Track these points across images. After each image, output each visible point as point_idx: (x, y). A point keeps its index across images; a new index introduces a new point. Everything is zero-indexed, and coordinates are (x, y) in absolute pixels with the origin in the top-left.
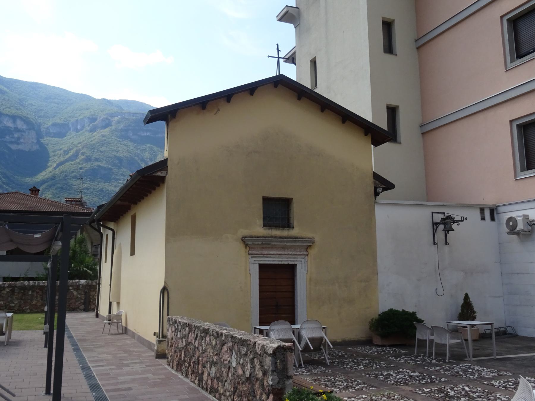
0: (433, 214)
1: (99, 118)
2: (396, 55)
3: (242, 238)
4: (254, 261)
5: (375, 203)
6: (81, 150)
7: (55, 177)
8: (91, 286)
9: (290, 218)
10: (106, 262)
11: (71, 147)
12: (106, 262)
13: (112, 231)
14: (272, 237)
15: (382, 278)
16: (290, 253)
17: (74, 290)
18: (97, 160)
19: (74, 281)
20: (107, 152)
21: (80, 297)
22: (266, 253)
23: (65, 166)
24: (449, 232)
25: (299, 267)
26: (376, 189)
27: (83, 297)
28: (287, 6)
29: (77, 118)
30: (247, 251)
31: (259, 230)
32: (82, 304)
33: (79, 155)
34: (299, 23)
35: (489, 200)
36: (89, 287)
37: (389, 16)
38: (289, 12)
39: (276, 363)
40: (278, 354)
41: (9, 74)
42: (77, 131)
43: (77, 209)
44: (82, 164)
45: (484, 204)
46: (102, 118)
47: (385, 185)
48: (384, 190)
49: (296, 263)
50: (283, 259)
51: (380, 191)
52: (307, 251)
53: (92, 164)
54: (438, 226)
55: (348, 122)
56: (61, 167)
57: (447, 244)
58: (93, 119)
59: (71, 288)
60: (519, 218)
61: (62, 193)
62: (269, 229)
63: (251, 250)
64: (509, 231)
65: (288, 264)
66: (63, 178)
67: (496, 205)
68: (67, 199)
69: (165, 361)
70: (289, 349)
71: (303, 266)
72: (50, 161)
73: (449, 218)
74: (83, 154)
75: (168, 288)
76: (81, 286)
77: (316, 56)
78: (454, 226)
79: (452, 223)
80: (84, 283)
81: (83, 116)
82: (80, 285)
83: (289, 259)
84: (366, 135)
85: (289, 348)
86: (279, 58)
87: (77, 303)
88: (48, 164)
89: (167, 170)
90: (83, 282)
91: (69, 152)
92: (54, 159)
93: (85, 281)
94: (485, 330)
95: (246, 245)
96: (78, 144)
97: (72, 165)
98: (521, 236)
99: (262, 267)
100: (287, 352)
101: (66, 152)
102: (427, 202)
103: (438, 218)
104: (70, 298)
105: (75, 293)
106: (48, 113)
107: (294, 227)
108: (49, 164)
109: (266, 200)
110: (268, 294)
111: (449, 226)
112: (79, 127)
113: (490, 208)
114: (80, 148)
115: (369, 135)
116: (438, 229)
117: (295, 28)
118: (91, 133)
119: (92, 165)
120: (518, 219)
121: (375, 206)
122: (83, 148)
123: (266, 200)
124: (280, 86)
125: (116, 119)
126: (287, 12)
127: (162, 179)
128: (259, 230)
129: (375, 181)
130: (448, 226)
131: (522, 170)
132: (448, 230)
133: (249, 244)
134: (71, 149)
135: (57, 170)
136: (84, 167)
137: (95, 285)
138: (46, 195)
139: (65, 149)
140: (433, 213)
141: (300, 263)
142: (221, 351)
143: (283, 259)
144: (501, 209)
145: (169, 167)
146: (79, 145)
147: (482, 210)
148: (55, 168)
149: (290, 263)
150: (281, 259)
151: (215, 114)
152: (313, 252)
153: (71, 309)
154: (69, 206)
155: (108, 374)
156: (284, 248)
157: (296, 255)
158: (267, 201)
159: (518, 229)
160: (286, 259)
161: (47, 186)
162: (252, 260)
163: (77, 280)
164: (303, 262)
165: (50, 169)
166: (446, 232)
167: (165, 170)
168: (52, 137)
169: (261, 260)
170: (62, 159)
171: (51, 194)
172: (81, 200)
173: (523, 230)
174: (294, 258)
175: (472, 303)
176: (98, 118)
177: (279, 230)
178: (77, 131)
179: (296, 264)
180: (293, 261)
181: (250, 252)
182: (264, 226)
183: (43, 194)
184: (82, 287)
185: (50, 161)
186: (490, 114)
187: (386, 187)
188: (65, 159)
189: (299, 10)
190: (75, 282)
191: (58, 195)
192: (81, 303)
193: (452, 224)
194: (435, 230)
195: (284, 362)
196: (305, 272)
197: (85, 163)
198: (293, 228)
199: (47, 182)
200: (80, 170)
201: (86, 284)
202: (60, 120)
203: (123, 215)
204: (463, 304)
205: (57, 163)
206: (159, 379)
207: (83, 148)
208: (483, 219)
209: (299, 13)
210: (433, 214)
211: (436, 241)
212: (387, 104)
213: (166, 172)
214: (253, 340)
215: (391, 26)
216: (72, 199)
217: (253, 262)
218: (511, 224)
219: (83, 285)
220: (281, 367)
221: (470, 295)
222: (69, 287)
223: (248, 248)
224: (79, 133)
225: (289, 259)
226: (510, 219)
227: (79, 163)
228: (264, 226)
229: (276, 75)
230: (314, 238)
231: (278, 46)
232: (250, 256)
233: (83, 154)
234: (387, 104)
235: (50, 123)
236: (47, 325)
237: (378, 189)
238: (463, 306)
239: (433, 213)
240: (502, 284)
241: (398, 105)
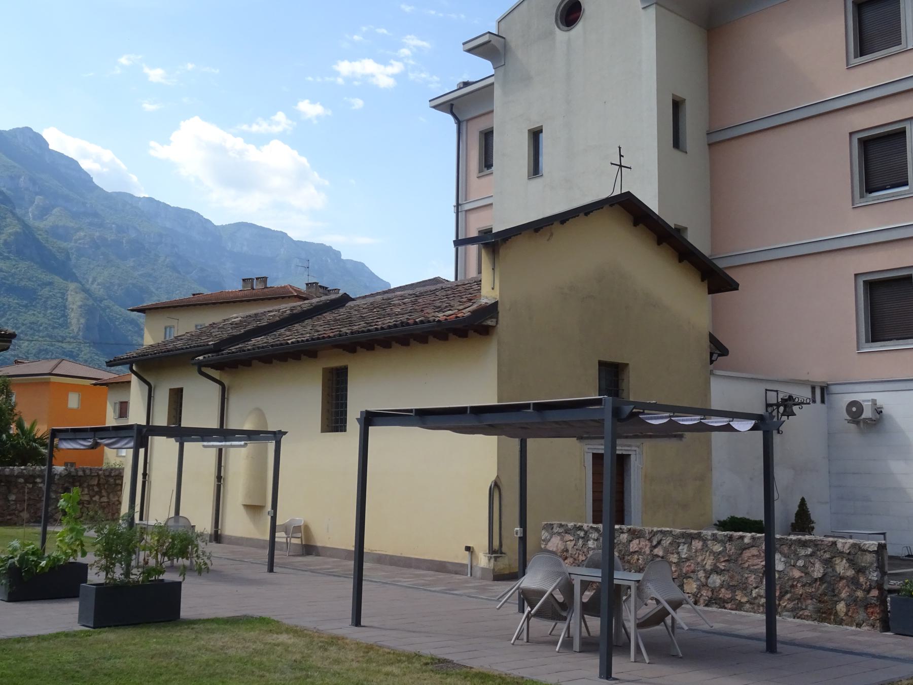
2: (686, 152)
5: (710, 374)
8: (76, 477)
9: (620, 391)
21: (54, 497)
24: (790, 417)
25: (633, 458)
26: (711, 354)
34: (505, 63)
35: (819, 375)
37: (680, 94)
38: (492, 42)
39: (879, 559)
45: (808, 380)
48: (719, 355)
49: (630, 453)
59: (38, 480)
64: (849, 418)
67: (828, 383)
73: (791, 398)
76: (57, 477)
78: (795, 409)
80: (63, 472)
82: (56, 474)
83: (623, 448)
84: (703, 280)
89: (497, 318)
98: (862, 424)
104: (37, 499)
113: (820, 386)
120: (864, 404)
121: (710, 378)
126: (488, 42)
131: (867, 341)
137: (83, 475)
140: (766, 390)
141: (634, 453)
142: (741, 553)
144: (834, 389)
145: (500, 314)
147: (813, 388)
151: (548, 240)
158: (603, 366)
159: (863, 416)
173: (871, 419)
179: (630, 455)
184: (58, 479)
186: (826, 260)
189: (505, 42)
196: (640, 465)
201: (66, 474)
204: (798, 511)
209: (505, 46)
210: (767, 392)
218: (854, 409)
219: (60, 475)
225: (623, 448)
226: (854, 403)
229: (620, 193)
238: (797, 515)
239: (766, 390)
240: (830, 486)
241: (684, 225)
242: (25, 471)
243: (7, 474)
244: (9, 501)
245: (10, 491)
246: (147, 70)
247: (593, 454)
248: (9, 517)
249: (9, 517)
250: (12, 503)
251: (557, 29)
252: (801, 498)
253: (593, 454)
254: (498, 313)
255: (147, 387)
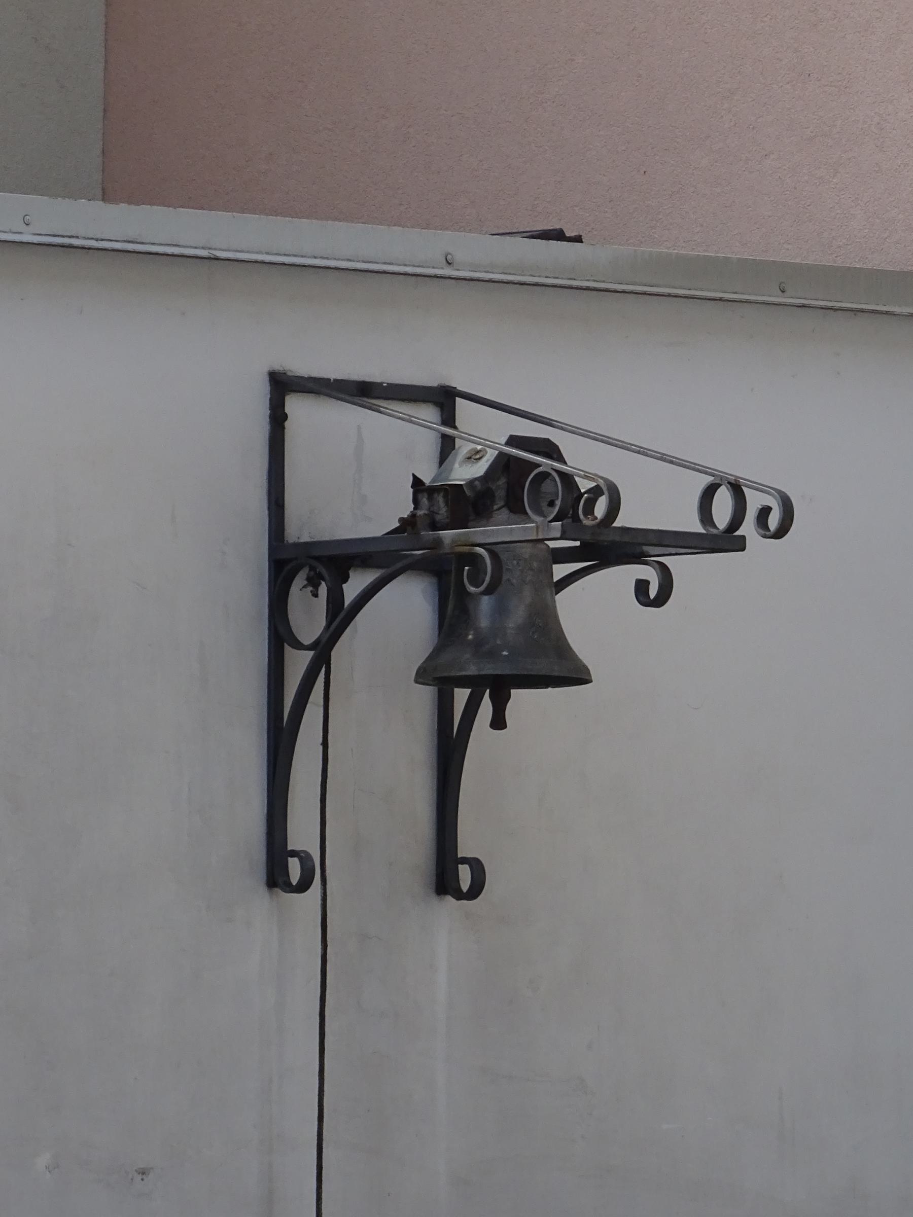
0: (295, 405)
24: (516, 694)
54: (352, 589)
77: (414, 475)
79: (561, 556)
102: (488, 574)
110: (514, 450)
111: (518, 615)
116: (337, 654)
130: (501, 610)
159: (442, 494)
166: (461, 696)
193: (560, 571)
210: (295, 405)
221: (416, 474)
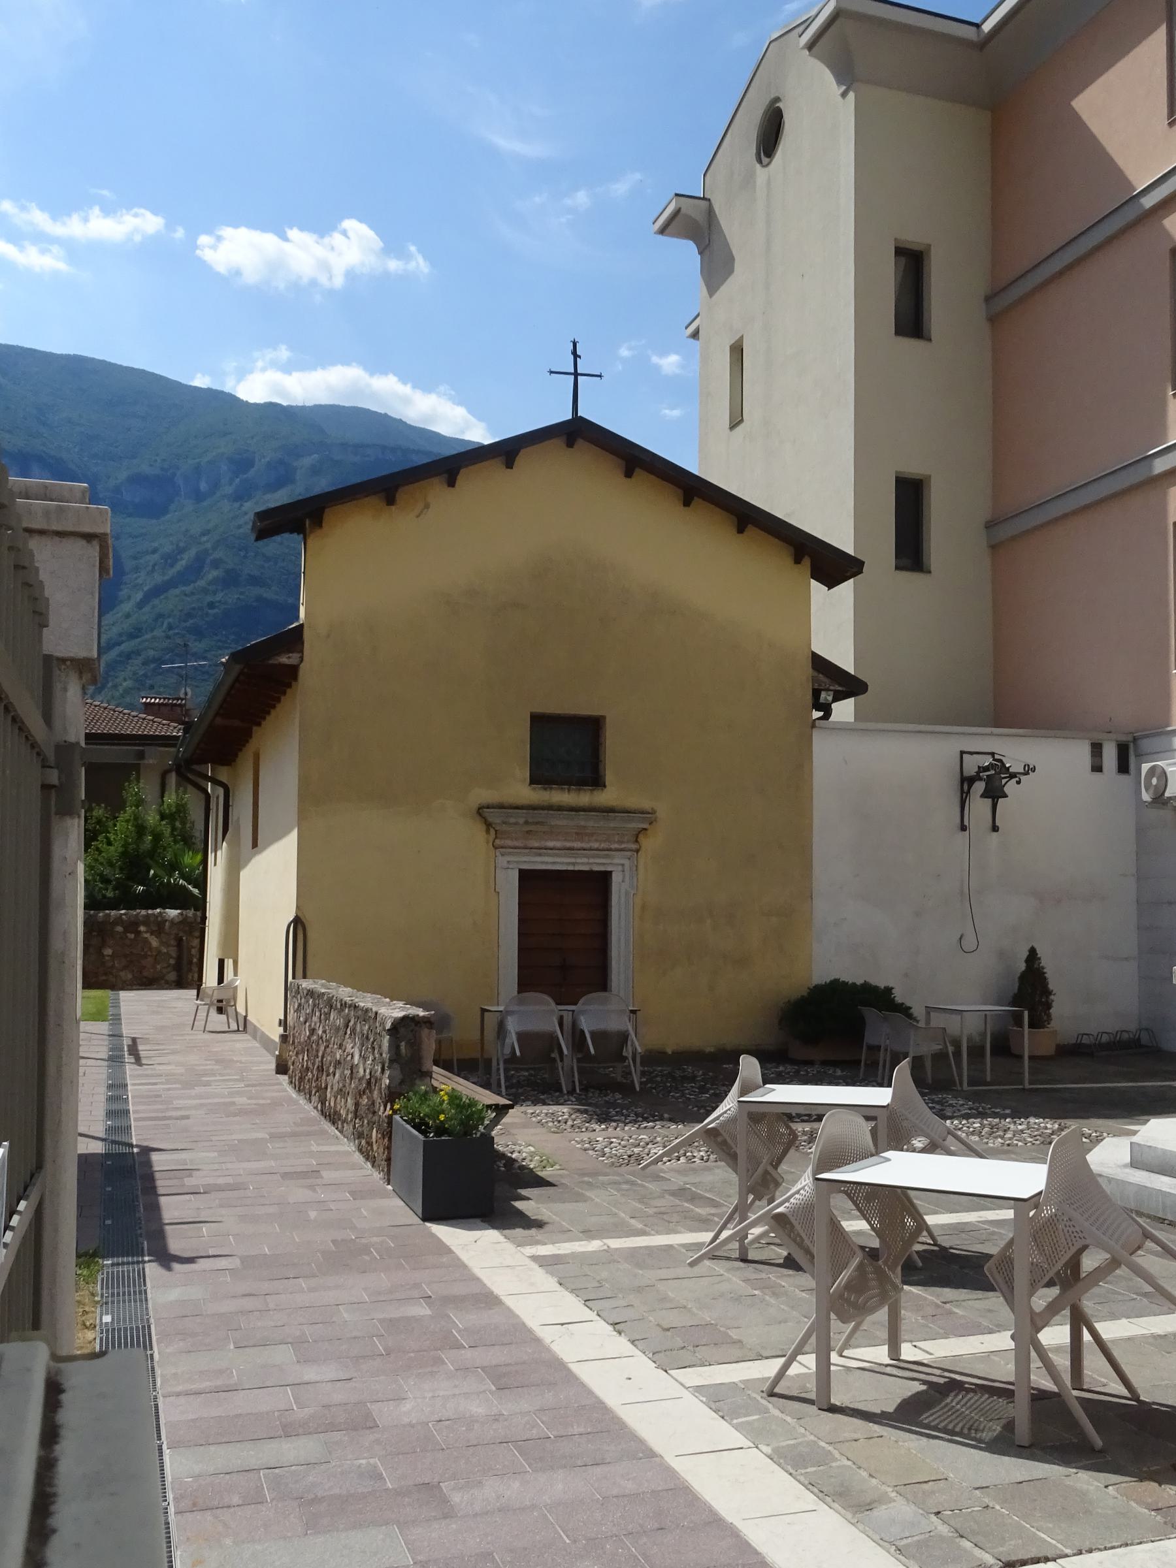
1: (260, 460)
3: (479, 809)
4: (508, 862)
6: (210, 552)
7: (140, 630)
10: (215, 865)
11: (182, 544)
12: (215, 865)
13: (222, 787)
14: (550, 808)
15: (821, 908)
16: (596, 845)
17: (152, 934)
18: (254, 581)
19: (150, 912)
20: (284, 560)
21: (165, 951)
22: (536, 844)
23: (166, 598)
25: (616, 878)
27: (173, 952)
28: (677, 195)
29: (197, 460)
30: (491, 840)
31: (526, 793)
32: (169, 969)
33: (206, 569)
36: (187, 928)
37: (914, 237)
38: (683, 211)
39: (398, 1047)
40: (402, 1030)
41: (3, 342)
42: (199, 497)
43: (165, 728)
44: (215, 593)
46: (268, 459)
47: (840, 685)
50: (579, 860)
51: (830, 698)
52: (637, 841)
53: (242, 593)
55: (751, 530)
56: (156, 601)
57: (995, 828)
58: (242, 463)
59: (142, 928)
60: (1171, 769)
61: (160, 677)
62: (545, 789)
63: (501, 839)
65: (591, 872)
66: (164, 632)
67: (1135, 735)
68: (148, 700)
69: (286, 1077)
70: (425, 1023)
71: (627, 879)
72: (126, 584)
74: (216, 564)
75: (304, 920)
81: (214, 454)
82: (166, 921)
83: (591, 861)
84: (798, 560)
85: (425, 1020)
86: (576, 374)
87: (159, 967)
88: (121, 593)
89: (302, 651)
90: (173, 913)
91: (179, 557)
92: (136, 579)
93: (179, 911)
94: (1080, 1037)
95: (488, 825)
96: (203, 534)
97: (186, 595)
99: (526, 877)
100: (421, 1027)
101: (170, 559)
103: (972, 765)
105: (154, 942)
106: (116, 447)
107: (607, 784)
108: (124, 592)
109: (539, 722)
112: (203, 486)
114: (209, 545)
115: (807, 562)
117: (700, 253)
118: (237, 505)
119: (242, 597)
122: (214, 548)
123: (539, 722)
124: (580, 443)
125: (307, 461)
127: (292, 672)
128: (522, 791)
129: (816, 674)
132: (994, 794)
133: (495, 824)
134: (181, 551)
135: (147, 609)
136: (220, 602)
138: (117, 680)
139: (168, 548)
140: (962, 753)
143: (579, 860)
146: (205, 539)
148: (141, 605)
149: (596, 868)
150: (573, 860)
152: (649, 844)
153: (144, 980)
154: (144, 719)
155: (160, 1096)
156: (580, 834)
157: (610, 850)
160: (585, 860)
161: (120, 655)
162: (502, 861)
163: (158, 910)
164: (627, 868)
165: (127, 607)
167: (299, 652)
168: (130, 515)
169: (525, 862)
170: (158, 578)
171: (130, 678)
172: (184, 702)
174: (607, 856)
175: (1045, 970)
176: (257, 460)
177: (569, 790)
178: (199, 497)
179: (611, 872)
180: (604, 864)
181: (498, 842)
182: (534, 781)
183: (110, 679)
184: (170, 928)
185: (126, 584)
187: (844, 689)
188: (166, 578)
190: (153, 914)
191: (151, 682)
192: (169, 965)
194: (964, 795)
195: (415, 1045)
197: (222, 591)
198: (605, 786)
199: (119, 644)
200: (210, 611)
202: (151, 465)
203: (241, 750)
205: (146, 589)
206: (255, 1104)
207: (214, 548)
208: (1097, 768)
209: (710, 213)
210: (964, 756)
211: (966, 823)
212: (896, 472)
213: (299, 655)
214: (374, 1009)
215: (922, 260)
216: (164, 699)
217: (505, 865)
219: (172, 921)
220: (409, 1055)
222: (139, 926)
223: (492, 832)
224: (205, 504)
225: (591, 861)
227: (205, 591)
228: (534, 781)
230: (653, 812)
231: (575, 344)
232: (497, 850)
233: (216, 564)
234: (896, 472)
235: (123, 475)
236: (299, 1121)
237: (823, 695)
238: (1023, 977)
239: (962, 753)
241: (927, 473)
242: (124, 917)
243: (100, 920)
244: (103, 956)
245: (103, 944)
246: (655, 359)
247: (521, 871)
248: (104, 978)
249: (104, 978)
250: (107, 958)
251: (758, 166)
252: (1029, 947)
253: (521, 871)
254: (303, 643)
255: (202, 796)
